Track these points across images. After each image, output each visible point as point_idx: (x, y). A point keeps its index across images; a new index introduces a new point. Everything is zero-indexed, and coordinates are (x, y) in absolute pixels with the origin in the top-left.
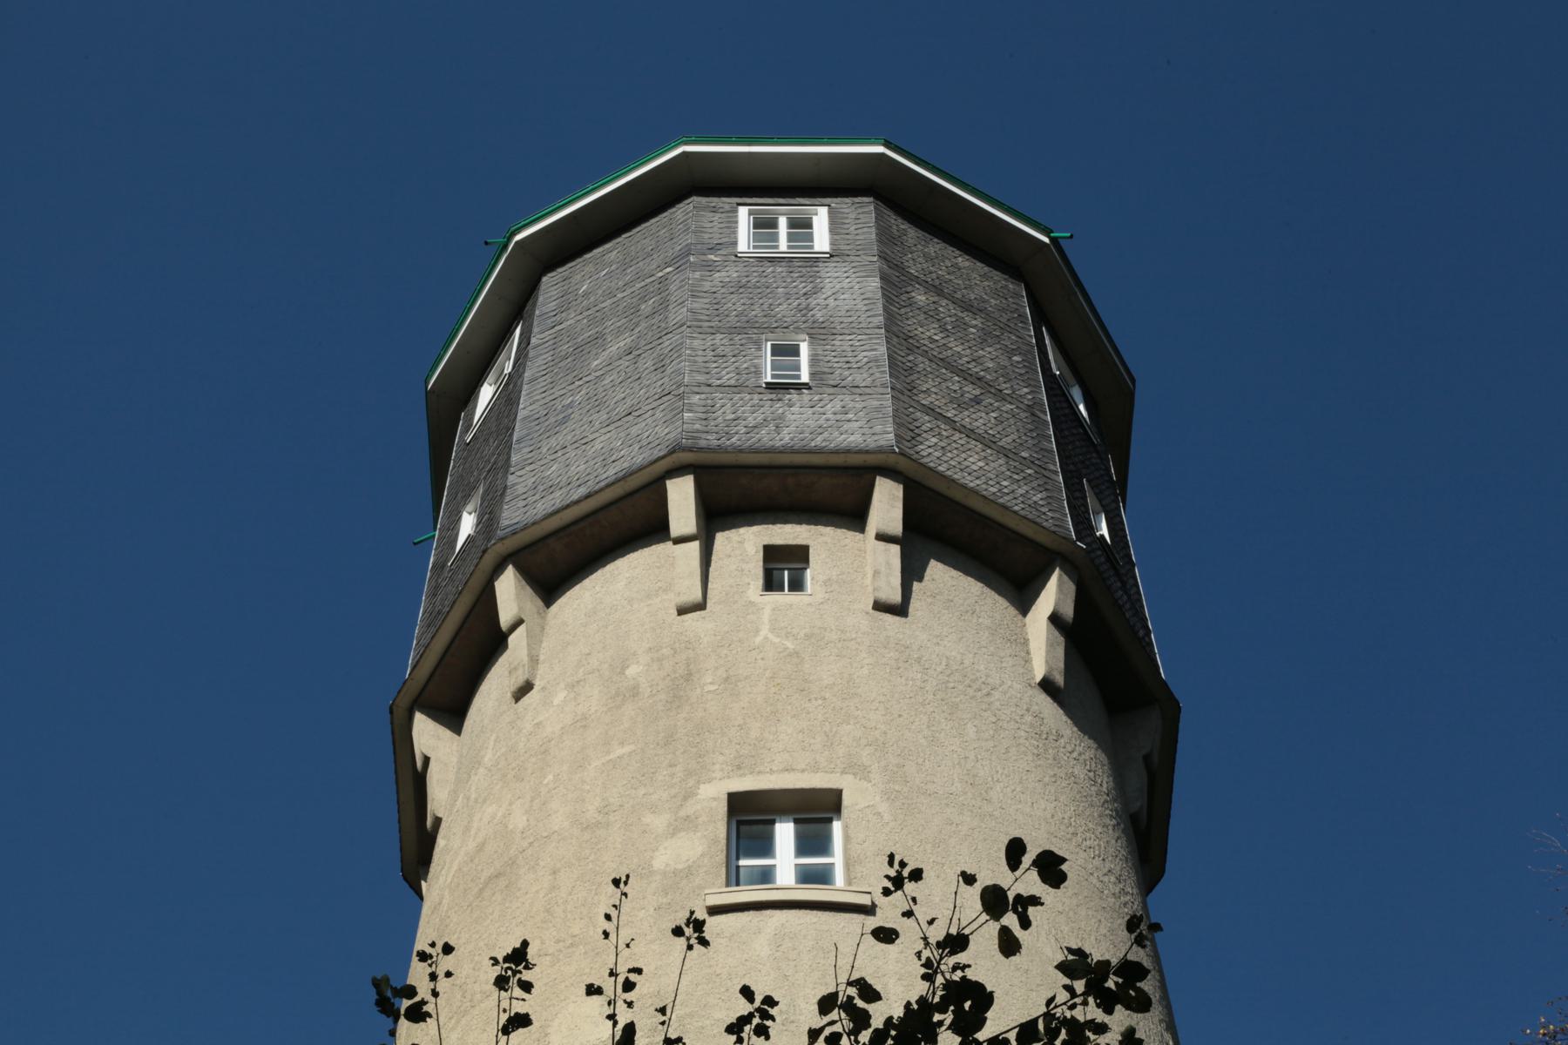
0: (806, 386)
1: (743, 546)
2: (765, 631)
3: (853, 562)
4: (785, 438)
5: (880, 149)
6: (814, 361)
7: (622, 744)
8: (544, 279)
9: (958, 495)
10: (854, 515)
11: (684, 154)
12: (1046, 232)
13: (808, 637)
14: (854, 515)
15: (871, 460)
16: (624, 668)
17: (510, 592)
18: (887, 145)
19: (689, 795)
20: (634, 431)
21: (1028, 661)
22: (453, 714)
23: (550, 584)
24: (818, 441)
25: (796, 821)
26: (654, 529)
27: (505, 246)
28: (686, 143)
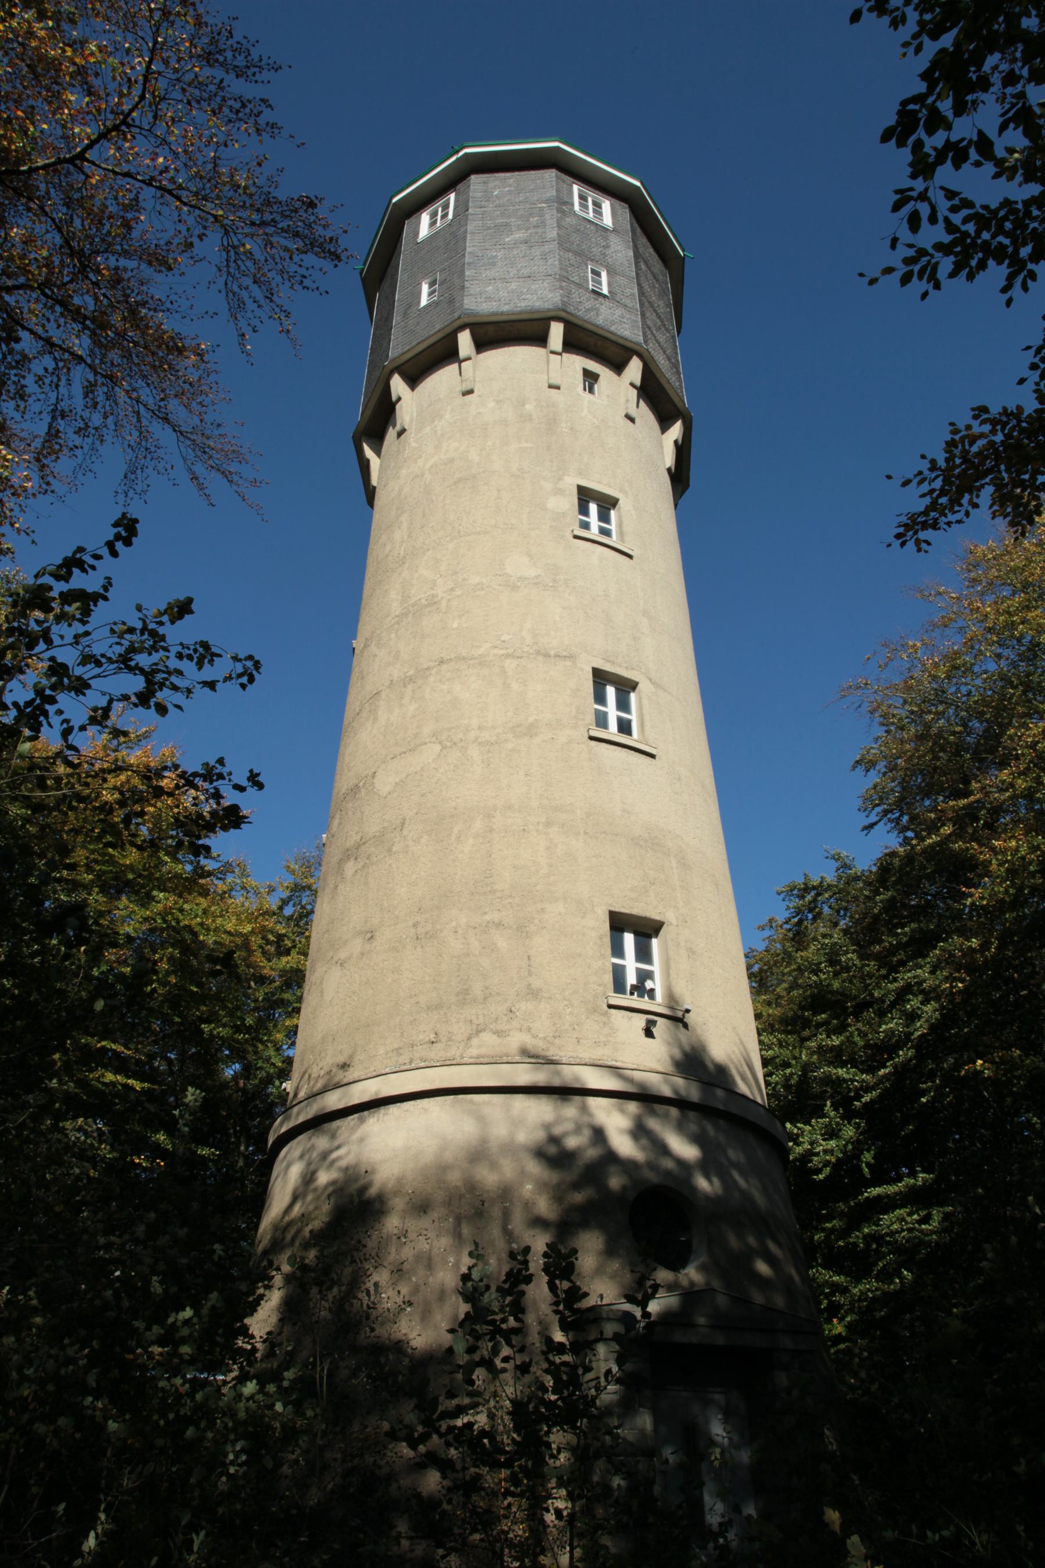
0: (604, 296)
1: (578, 363)
2: (585, 412)
3: (619, 389)
4: (600, 321)
5: (638, 184)
6: (609, 284)
7: (527, 441)
8: (473, 177)
9: (658, 375)
10: (618, 367)
11: (558, 148)
12: (683, 251)
13: (602, 421)
14: (618, 367)
15: (550, 314)
16: (523, 405)
17: (465, 341)
18: (642, 183)
19: (560, 479)
20: (533, 287)
21: (663, 458)
22: (413, 381)
23: (482, 345)
24: (613, 329)
25: (598, 506)
26: (540, 339)
27: (458, 152)
28: (563, 143)
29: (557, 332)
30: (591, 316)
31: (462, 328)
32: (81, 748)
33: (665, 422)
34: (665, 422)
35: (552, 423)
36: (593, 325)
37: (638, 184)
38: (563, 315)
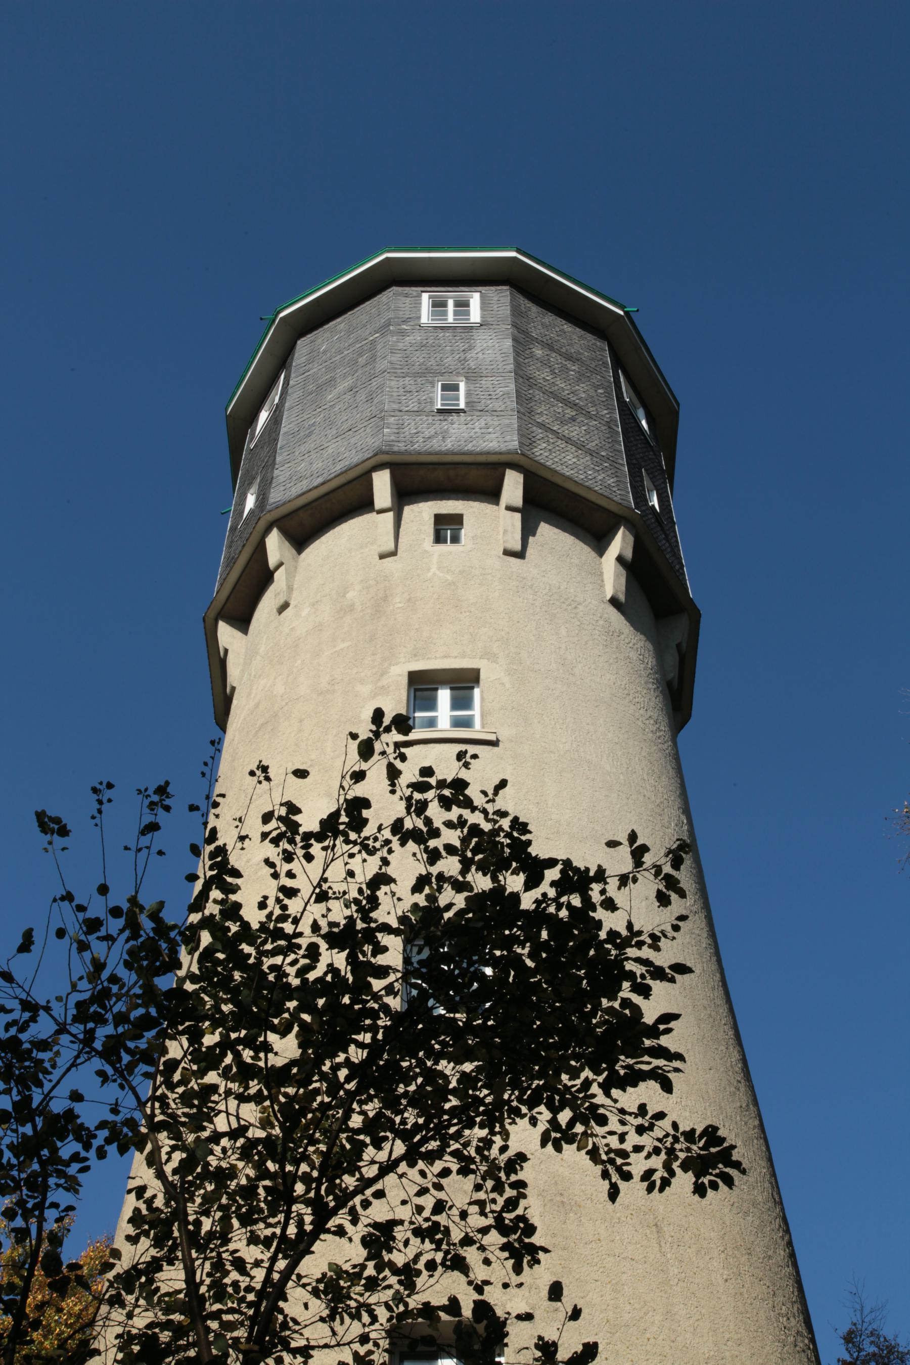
0: (463, 411)
1: (421, 514)
3: (491, 524)
4: (448, 445)
7: (343, 641)
11: (387, 258)
13: (461, 572)
18: (519, 251)
20: (353, 441)
23: (300, 541)
24: (470, 447)
25: (452, 689)
27: (274, 321)
28: (389, 251)
29: (513, 487)
30: (436, 444)
31: (268, 531)
32: (512, 1136)
33: (599, 541)
34: (599, 541)
35: (380, 604)
36: (430, 454)
37: (513, 254)
38: (523, 461)
